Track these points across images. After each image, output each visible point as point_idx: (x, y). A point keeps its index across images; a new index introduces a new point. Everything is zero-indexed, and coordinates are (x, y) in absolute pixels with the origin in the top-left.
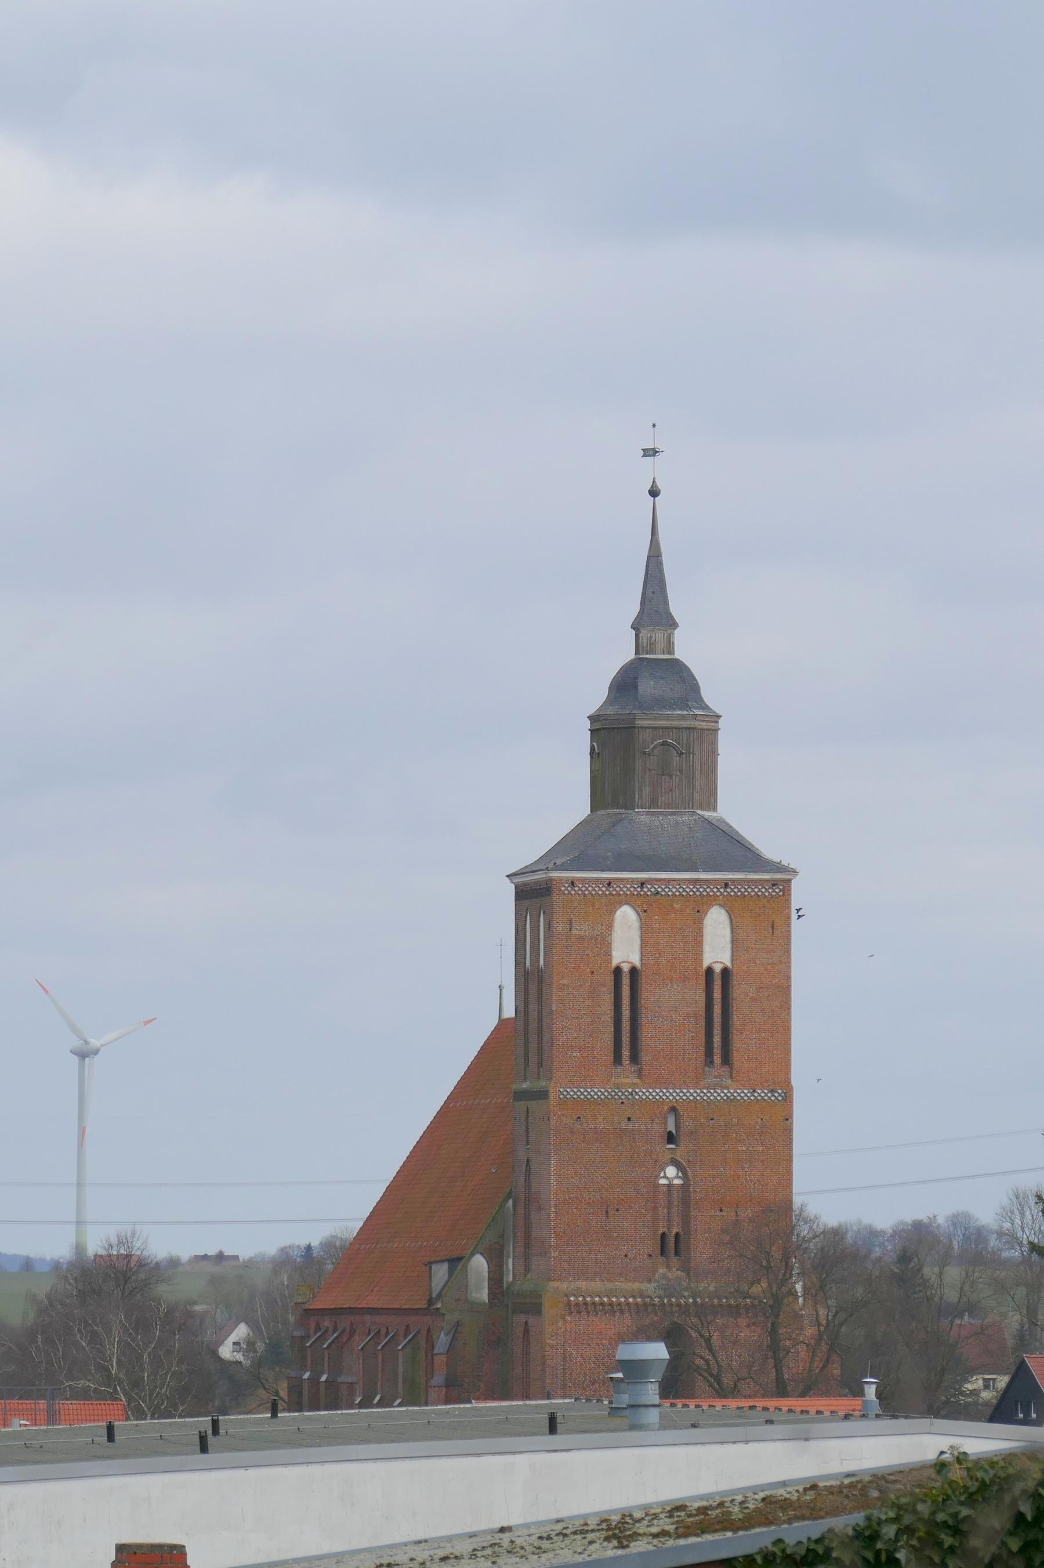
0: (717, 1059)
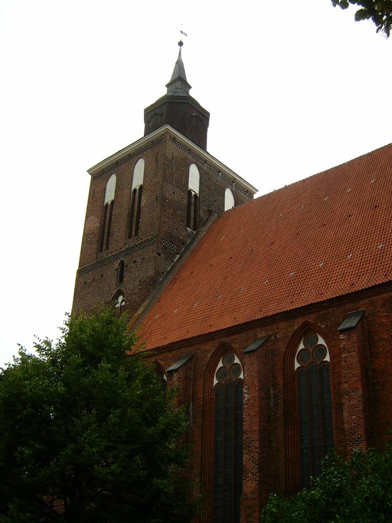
0: (104, 247)
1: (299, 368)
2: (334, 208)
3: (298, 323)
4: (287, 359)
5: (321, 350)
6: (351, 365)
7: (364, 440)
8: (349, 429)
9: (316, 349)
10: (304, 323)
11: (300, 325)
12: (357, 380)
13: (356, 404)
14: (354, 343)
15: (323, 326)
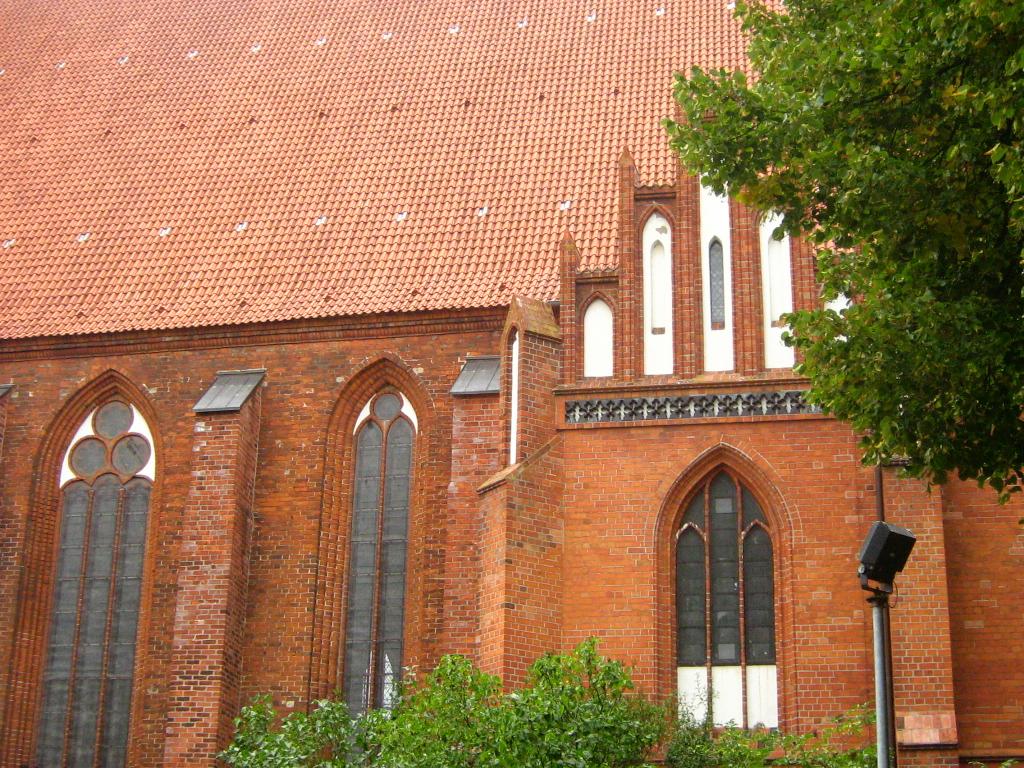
1: (72, 482)
2: (213, 87)
3: (88, 370)
4: (45, 456)
5: (134, 442)
6: (212, 498)
7: (216, 678)
8: (186, 647)
9: (124, 443)
10: (104, 373)
11: (92, 378)
12: (222, 537)
13: (212, 592)
14: (230, 447)
15: (153, 391)
